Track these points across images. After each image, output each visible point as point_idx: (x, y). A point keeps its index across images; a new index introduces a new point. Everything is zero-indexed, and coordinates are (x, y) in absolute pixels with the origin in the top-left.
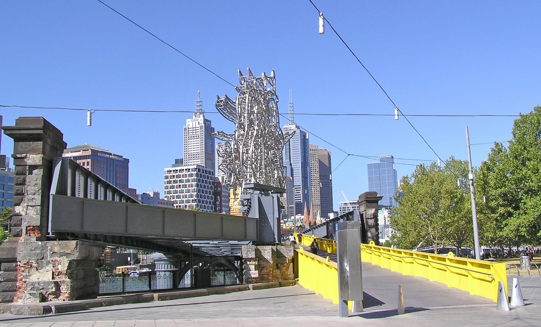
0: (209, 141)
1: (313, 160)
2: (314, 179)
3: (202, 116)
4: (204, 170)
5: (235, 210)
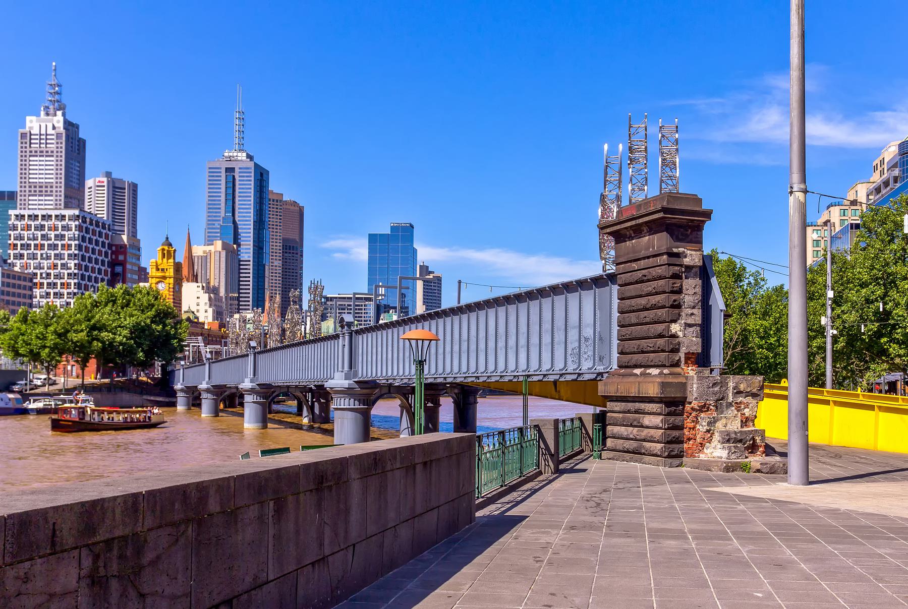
0: (74, 163)
3: (59, 113)
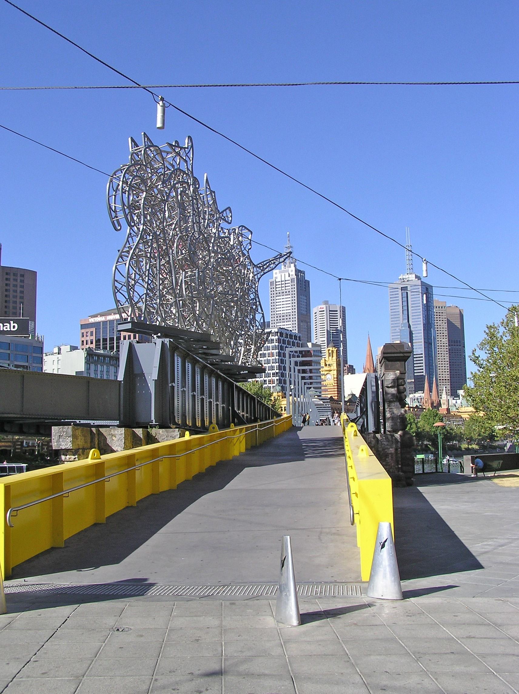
1: (440, 320)
2: (441, 346)
3: (292, 265)
4: (287, 334)
5: (329, 386)
